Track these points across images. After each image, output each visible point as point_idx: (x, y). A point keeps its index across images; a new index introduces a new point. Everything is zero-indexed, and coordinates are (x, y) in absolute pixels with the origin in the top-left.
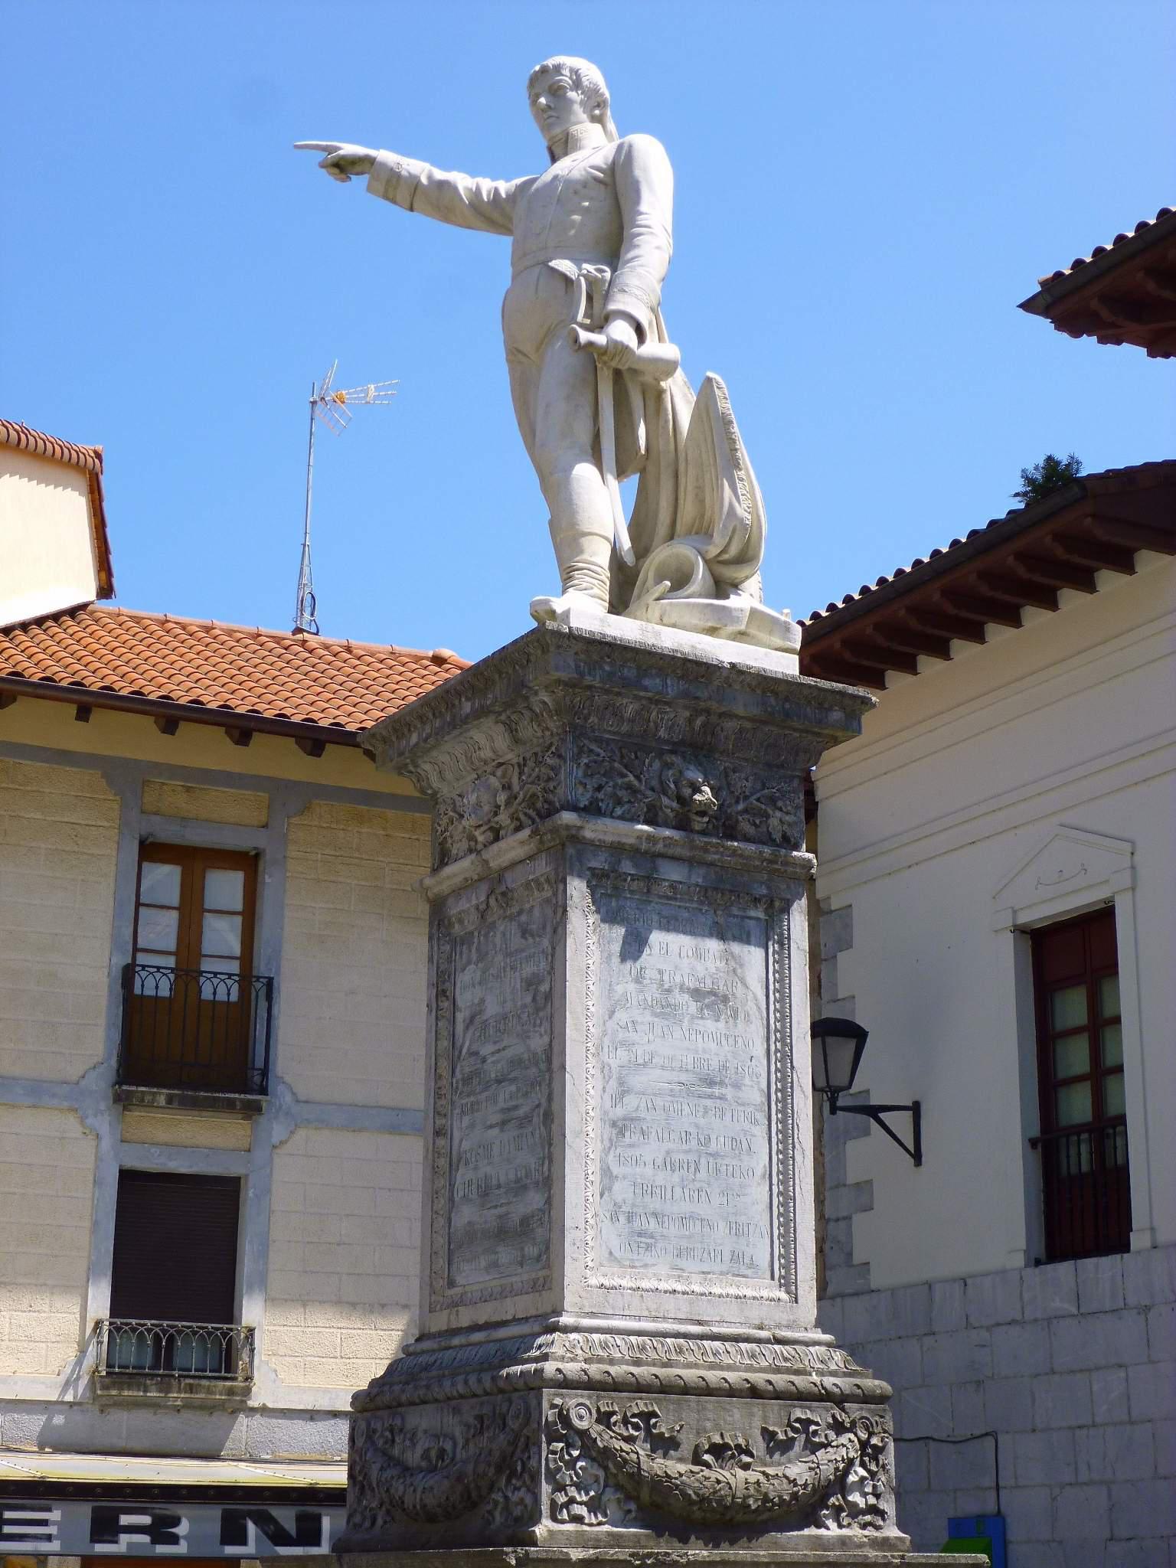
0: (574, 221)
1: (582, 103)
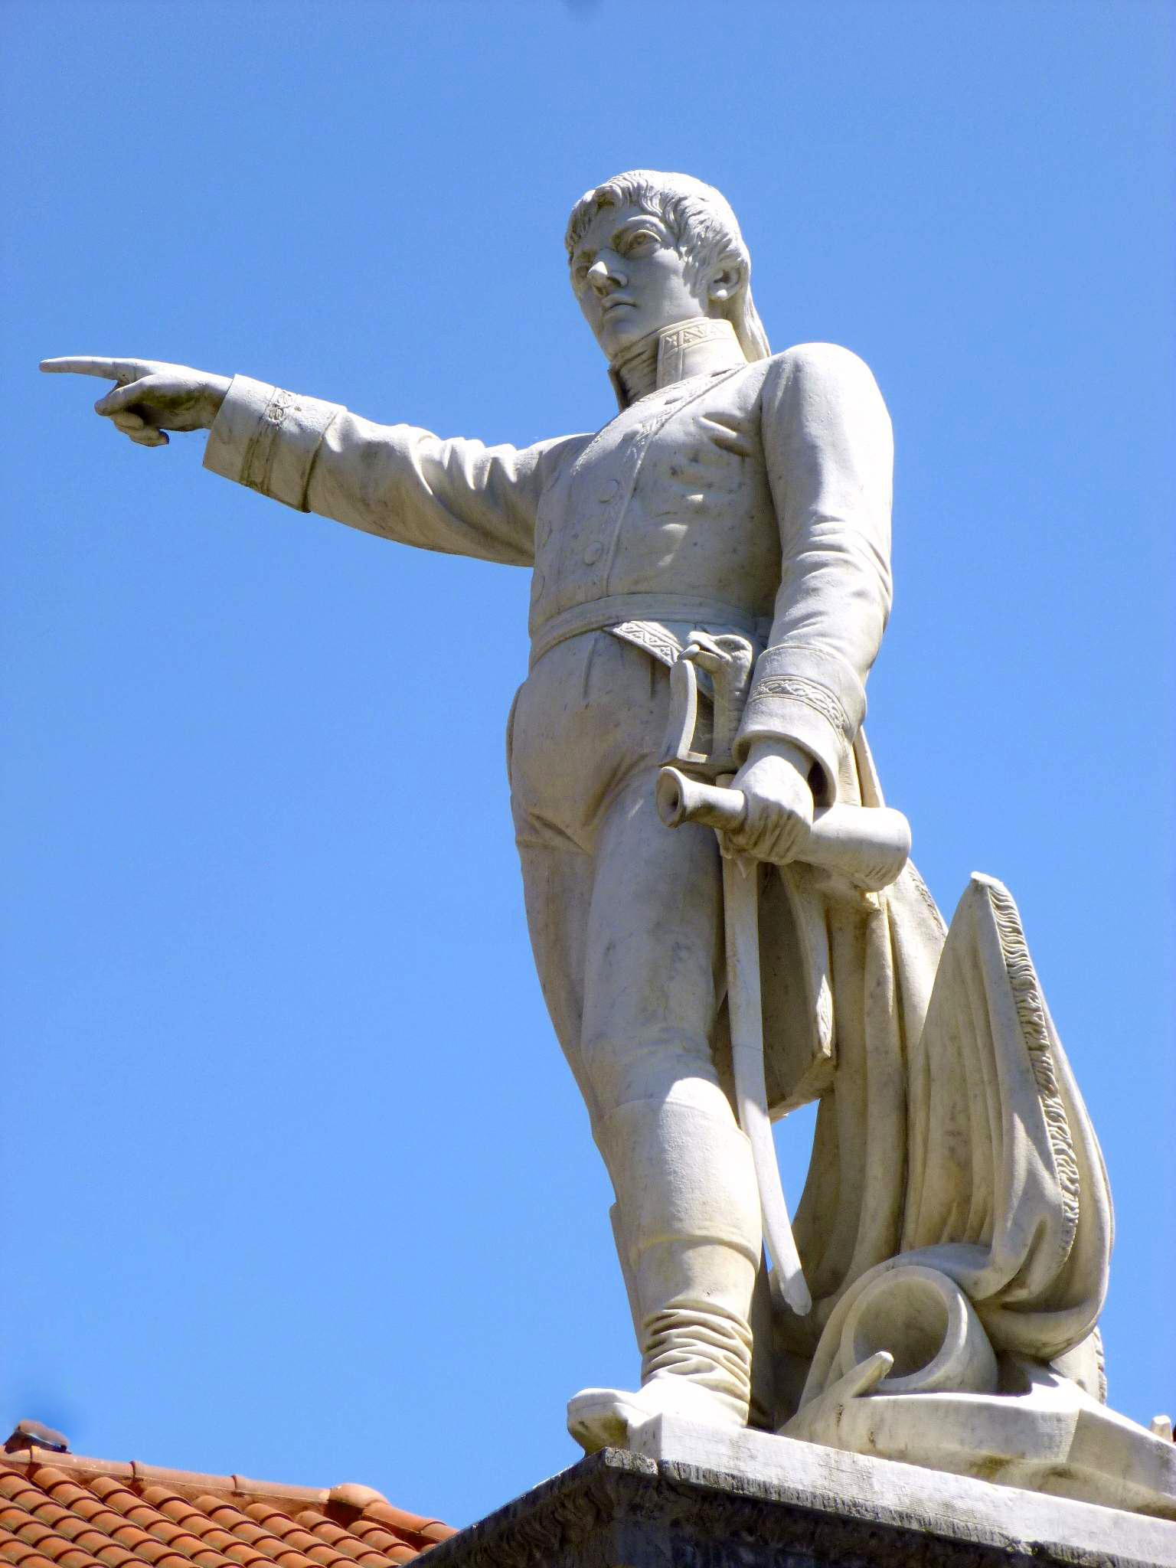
0: (670, 535)
1: (688, 274)
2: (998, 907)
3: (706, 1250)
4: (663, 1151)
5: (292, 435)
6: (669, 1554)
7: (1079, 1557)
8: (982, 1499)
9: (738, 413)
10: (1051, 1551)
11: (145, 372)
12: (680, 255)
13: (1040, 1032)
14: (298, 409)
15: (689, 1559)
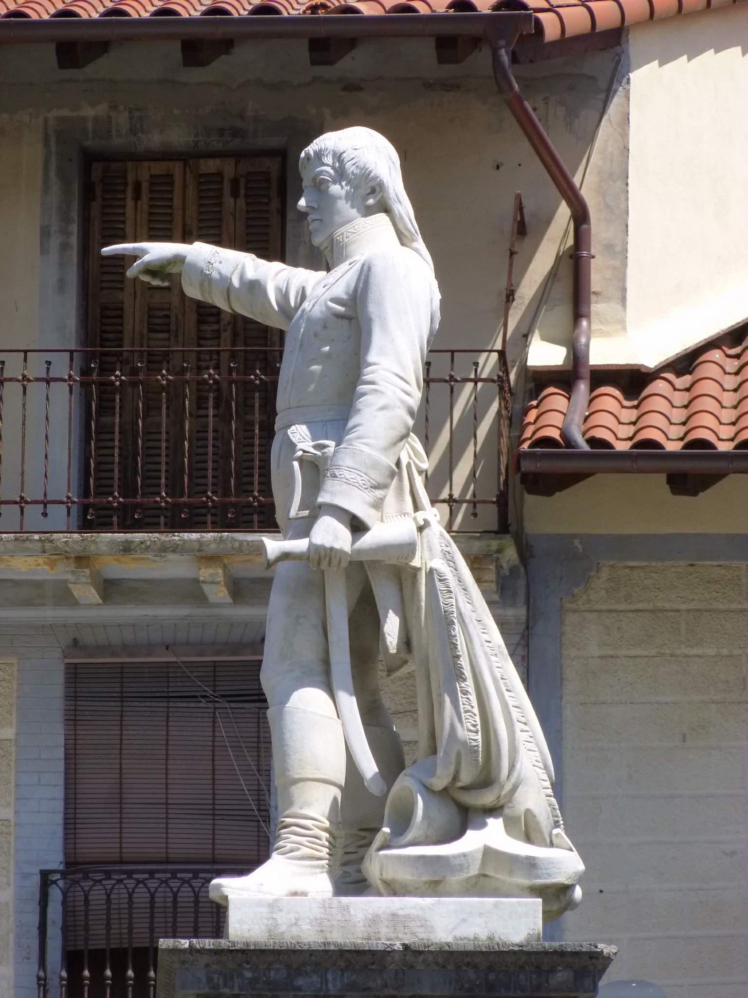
0: (313, 373)
1: (348, 197)
2: (440, 580)
3: (300, 785)
4: (283, 733)
5: (217, 280)
6: (204, 980)
7: (429, 946)
8: (415, 907)
9: (345, 297)
10: (412, 947)
11: (145, 252)
12: (342, 187)
13: (457, 648)
14: (220, 262)
15: (216, 980)
